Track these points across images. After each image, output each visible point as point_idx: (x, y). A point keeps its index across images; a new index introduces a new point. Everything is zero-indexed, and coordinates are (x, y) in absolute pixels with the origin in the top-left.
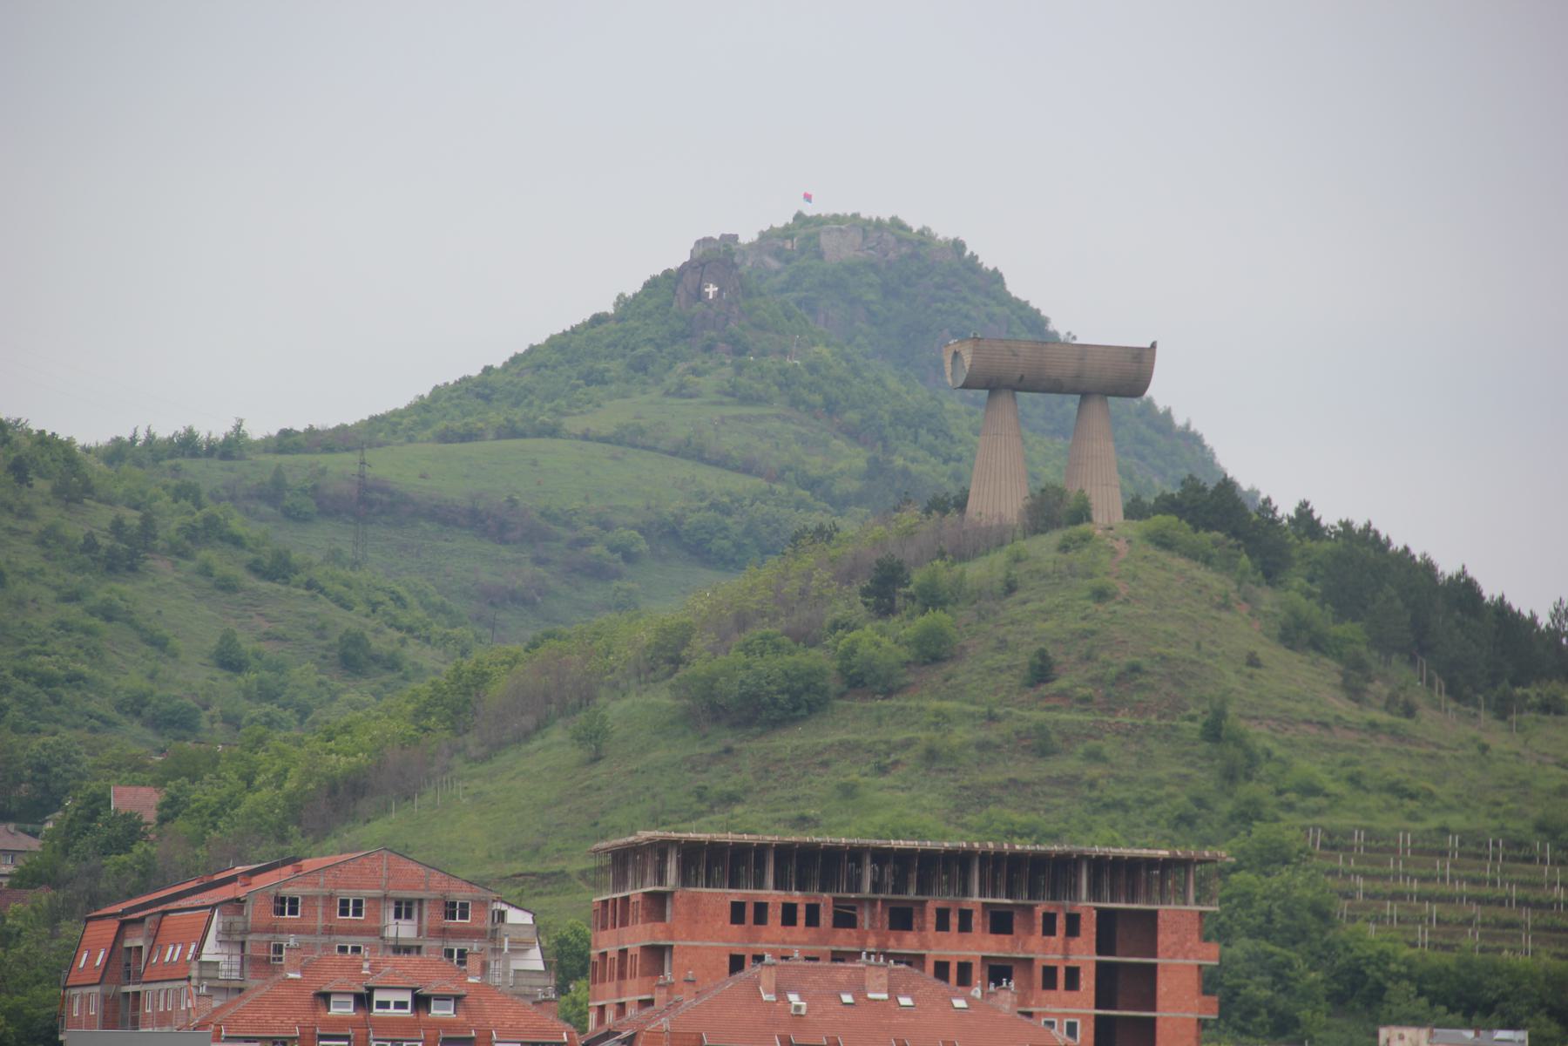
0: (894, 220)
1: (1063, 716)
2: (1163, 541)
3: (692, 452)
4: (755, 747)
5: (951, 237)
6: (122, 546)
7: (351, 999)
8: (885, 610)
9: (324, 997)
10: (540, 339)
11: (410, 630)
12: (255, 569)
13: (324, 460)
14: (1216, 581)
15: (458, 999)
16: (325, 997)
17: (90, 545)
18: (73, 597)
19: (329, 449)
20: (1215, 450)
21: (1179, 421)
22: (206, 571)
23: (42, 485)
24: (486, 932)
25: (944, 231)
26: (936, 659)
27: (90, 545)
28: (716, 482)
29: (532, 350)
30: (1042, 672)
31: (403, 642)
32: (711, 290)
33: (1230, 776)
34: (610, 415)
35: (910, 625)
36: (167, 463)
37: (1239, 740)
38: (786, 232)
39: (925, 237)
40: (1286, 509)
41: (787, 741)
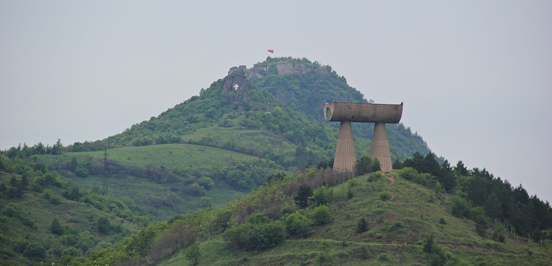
3: (230, 147)
11: (125, 217)
12: (66, 195)
13: (91, 154)
14: (427, 192)
19: (93, 150)
22: (47, 197)
25: (323, 63)
30: (363, 227)
31: (122, 222)
35: (313, 211)
37: (438, 252)
38: (264, 64)
39: (316, 65)
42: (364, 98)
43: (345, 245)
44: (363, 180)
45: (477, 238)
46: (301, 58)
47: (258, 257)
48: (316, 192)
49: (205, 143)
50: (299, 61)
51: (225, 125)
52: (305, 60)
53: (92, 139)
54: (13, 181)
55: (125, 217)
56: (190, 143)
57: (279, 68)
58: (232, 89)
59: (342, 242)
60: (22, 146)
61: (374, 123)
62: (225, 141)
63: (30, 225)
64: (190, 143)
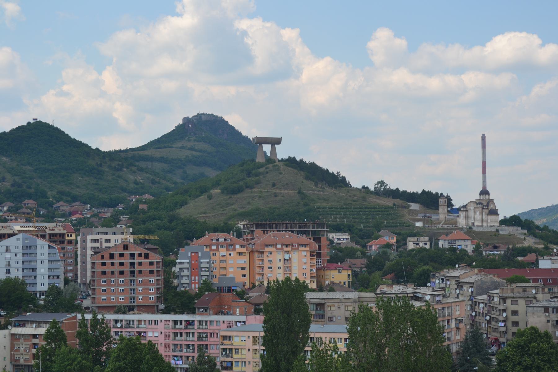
0: (423, 191)
1: (278, 191)
2: (287, 165)
3: (192, 149)
4: (235, 197)
5: (221, 116)
6: (119, 167)
7: (543, 309)
8: (249, 176)
9: (212, 240)
10: (165, 133)
11: (160, 178)
12: (138, 169)
13: (134, 152)
14: (295, 171)
15: (230, 239)
16: (212, 240)
17: (115, 167)
18: (114, 175)
19: (135, 151)
20: (315, 162)
21: (401, 189)
22: (131, 170)
23: (107, 159)
24: (321, 251)
25: (219, 115)
26: (258, 184)
27: (115, 167)
28: (196, 154)
29: (165, 135)
30: (274, 185)
31: (160, 180)
32: (190, 126)
33: (302, 199)
34: (179, 144)
35: (254, 179)
36: (118, 154)
37: (303, 194)
38: (196, 116)
39: (217, 116)
40: (326, 169)
41: (239, 195)
42: (434, 193)
43: (268, 192)
44: (270, 166)
45: (314, 187)
46: (211, 114)
47: (235, 196)
48: (253, 172)
49: (182, 147)
50: (210, 114)
51: (189, 141)
52: (212, 114)
53: (410, 190)
54: (118, 165)
55: (160, 178)
56: (176, 148)
57: (203, 117)
58: (188, 126)
59: (267, 190)
60: (114, 150)
61: (270, 145)
62: (189, 147)
63: (126, 181)
64: (176, 148)
